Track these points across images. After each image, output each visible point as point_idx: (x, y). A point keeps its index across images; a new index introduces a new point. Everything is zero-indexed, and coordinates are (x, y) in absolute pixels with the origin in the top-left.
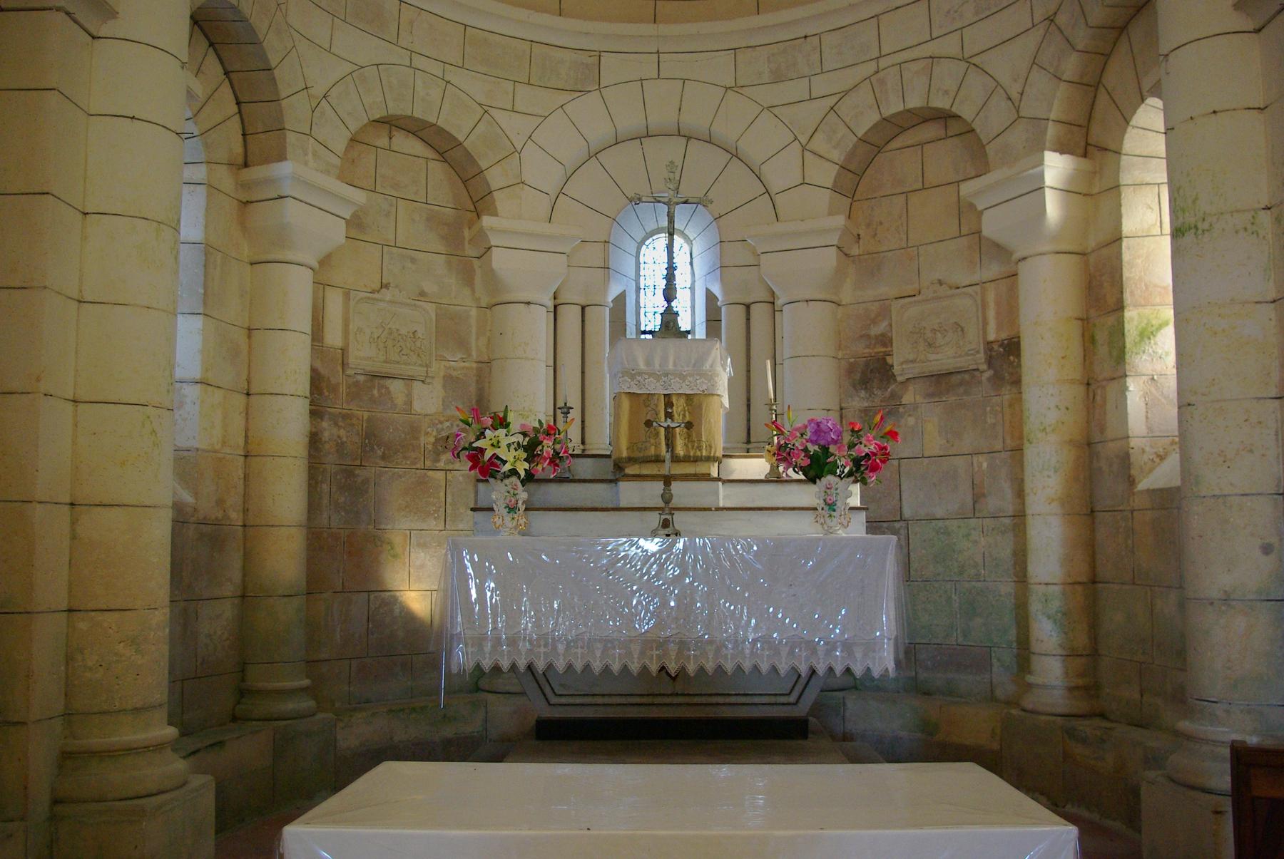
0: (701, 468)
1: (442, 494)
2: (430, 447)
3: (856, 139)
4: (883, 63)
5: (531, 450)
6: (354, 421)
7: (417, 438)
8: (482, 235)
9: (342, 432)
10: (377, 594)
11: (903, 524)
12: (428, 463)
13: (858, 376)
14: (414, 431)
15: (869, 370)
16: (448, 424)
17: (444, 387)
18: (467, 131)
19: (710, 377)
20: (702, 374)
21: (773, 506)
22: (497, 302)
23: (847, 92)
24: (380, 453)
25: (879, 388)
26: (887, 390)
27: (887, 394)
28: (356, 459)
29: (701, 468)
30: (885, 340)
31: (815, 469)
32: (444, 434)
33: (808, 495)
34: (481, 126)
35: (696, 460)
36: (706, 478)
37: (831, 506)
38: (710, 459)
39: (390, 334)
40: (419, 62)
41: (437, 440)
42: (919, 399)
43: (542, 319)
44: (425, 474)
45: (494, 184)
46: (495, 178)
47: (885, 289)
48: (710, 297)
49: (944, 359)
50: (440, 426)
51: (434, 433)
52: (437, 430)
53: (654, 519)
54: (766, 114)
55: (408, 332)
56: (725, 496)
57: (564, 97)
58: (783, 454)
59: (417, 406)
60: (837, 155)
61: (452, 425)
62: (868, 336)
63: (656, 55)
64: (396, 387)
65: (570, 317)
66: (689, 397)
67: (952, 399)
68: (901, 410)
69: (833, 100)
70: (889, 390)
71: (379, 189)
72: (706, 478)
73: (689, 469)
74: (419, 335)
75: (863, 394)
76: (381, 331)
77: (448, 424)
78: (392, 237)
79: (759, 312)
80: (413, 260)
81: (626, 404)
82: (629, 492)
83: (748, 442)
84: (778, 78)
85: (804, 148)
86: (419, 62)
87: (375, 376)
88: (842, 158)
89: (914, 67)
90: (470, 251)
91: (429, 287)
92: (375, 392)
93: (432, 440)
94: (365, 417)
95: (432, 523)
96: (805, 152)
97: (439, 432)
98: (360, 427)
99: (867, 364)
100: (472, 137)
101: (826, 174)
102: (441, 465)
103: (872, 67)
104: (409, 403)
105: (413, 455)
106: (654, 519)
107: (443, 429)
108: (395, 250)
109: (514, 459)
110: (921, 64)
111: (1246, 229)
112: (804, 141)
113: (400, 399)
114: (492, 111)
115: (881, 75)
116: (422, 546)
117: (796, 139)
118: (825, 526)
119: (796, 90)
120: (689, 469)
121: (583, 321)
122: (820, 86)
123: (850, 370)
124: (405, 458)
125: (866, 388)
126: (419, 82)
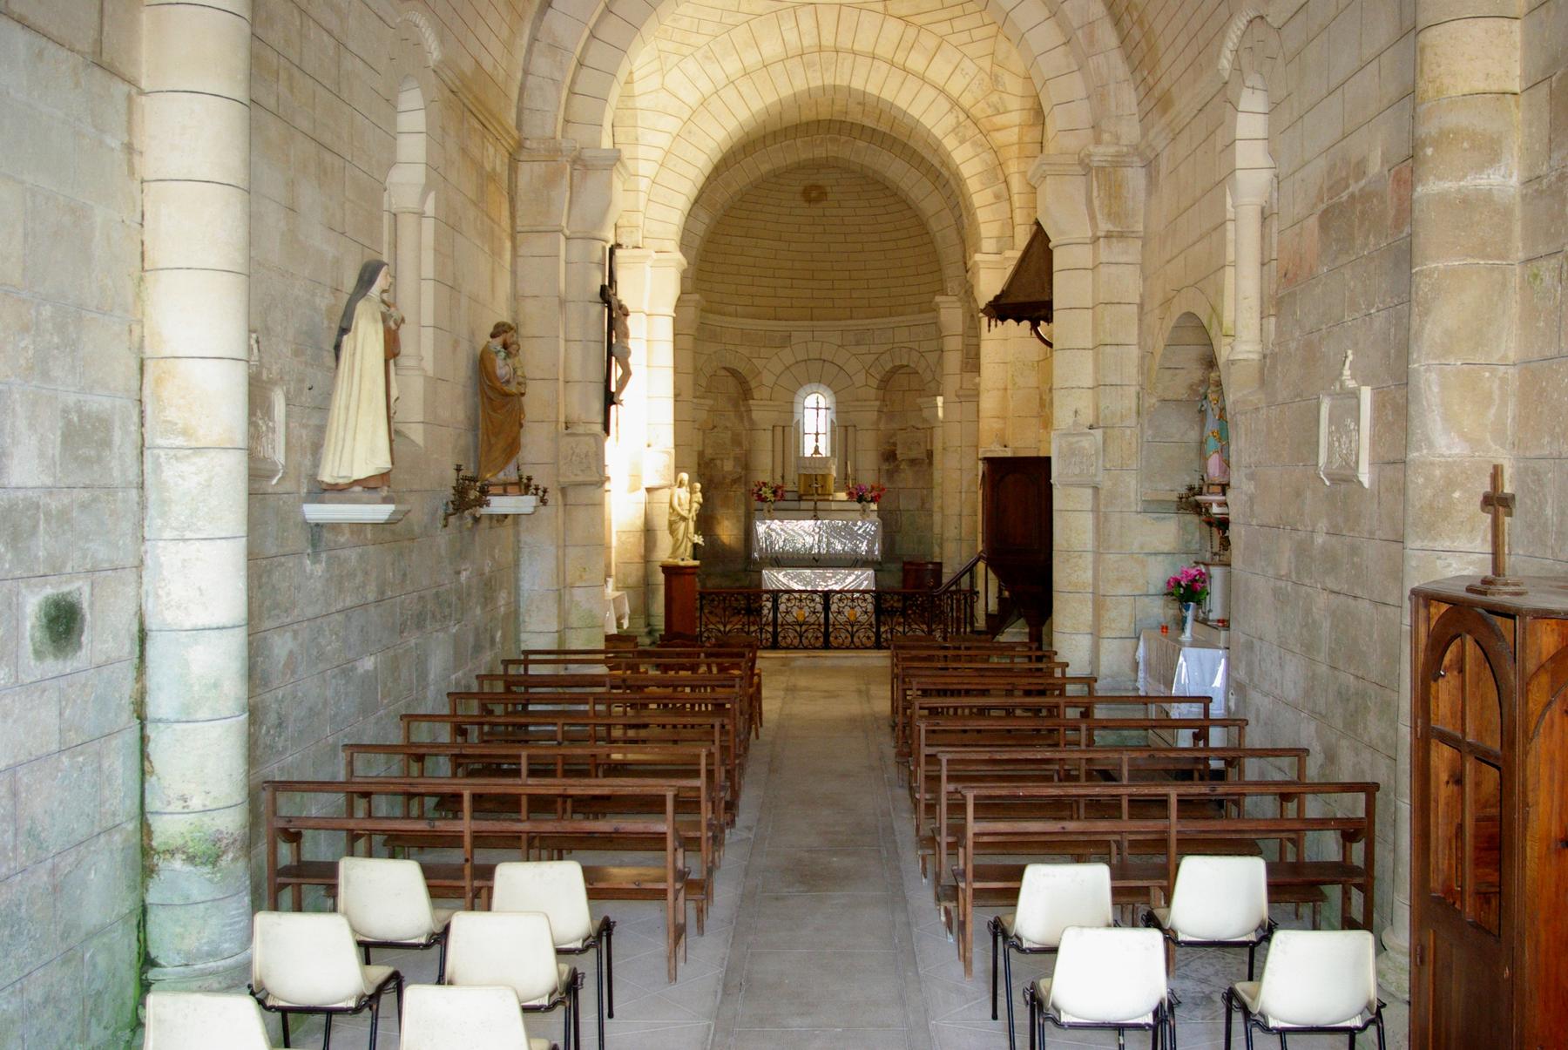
0: (826, 497)
5: (775, 493)
8: (749, 406)
19: (829, 469)
20: (826, 468)
22: (753, 427)
29: (826, 497)
30: (895, 444)
31: (860, 499)
33: (857, 506)
35: (824, 495)
36: (828, 500)
37: (864, 511)
38: (829, 495)
40: (728, 347)
43: (769, 434)
45: (753, 386)
46: (753, 384)
47: (895, 426)
48: (832, 421)
49: (913, 454)
53: (812, 513)
56: (834, 506)
57: (775, 351)
58: (850, 494)
60: (878, 376)
64: (718, 462)
65: (779, 431)
66: (823, 475)
72: (828, 500)
73: (822, 498)
79: (851, 430)
81: (803, 478)
82: (804, 505)
84: (858, 344)
85: (867, 372)
86: (728, 347)
87: (713, 459)
89: (905, 350)
90: (743, 409)
91: (729, 425)
95: (730, 511)
101: (874, 383)
106: (812, 513)
109: (770, 496)
116: (727, 519)
118: (1265, 267)
119: (863, 349)
120: (822, 498)
122: (874, 349)
123: (883, 454)
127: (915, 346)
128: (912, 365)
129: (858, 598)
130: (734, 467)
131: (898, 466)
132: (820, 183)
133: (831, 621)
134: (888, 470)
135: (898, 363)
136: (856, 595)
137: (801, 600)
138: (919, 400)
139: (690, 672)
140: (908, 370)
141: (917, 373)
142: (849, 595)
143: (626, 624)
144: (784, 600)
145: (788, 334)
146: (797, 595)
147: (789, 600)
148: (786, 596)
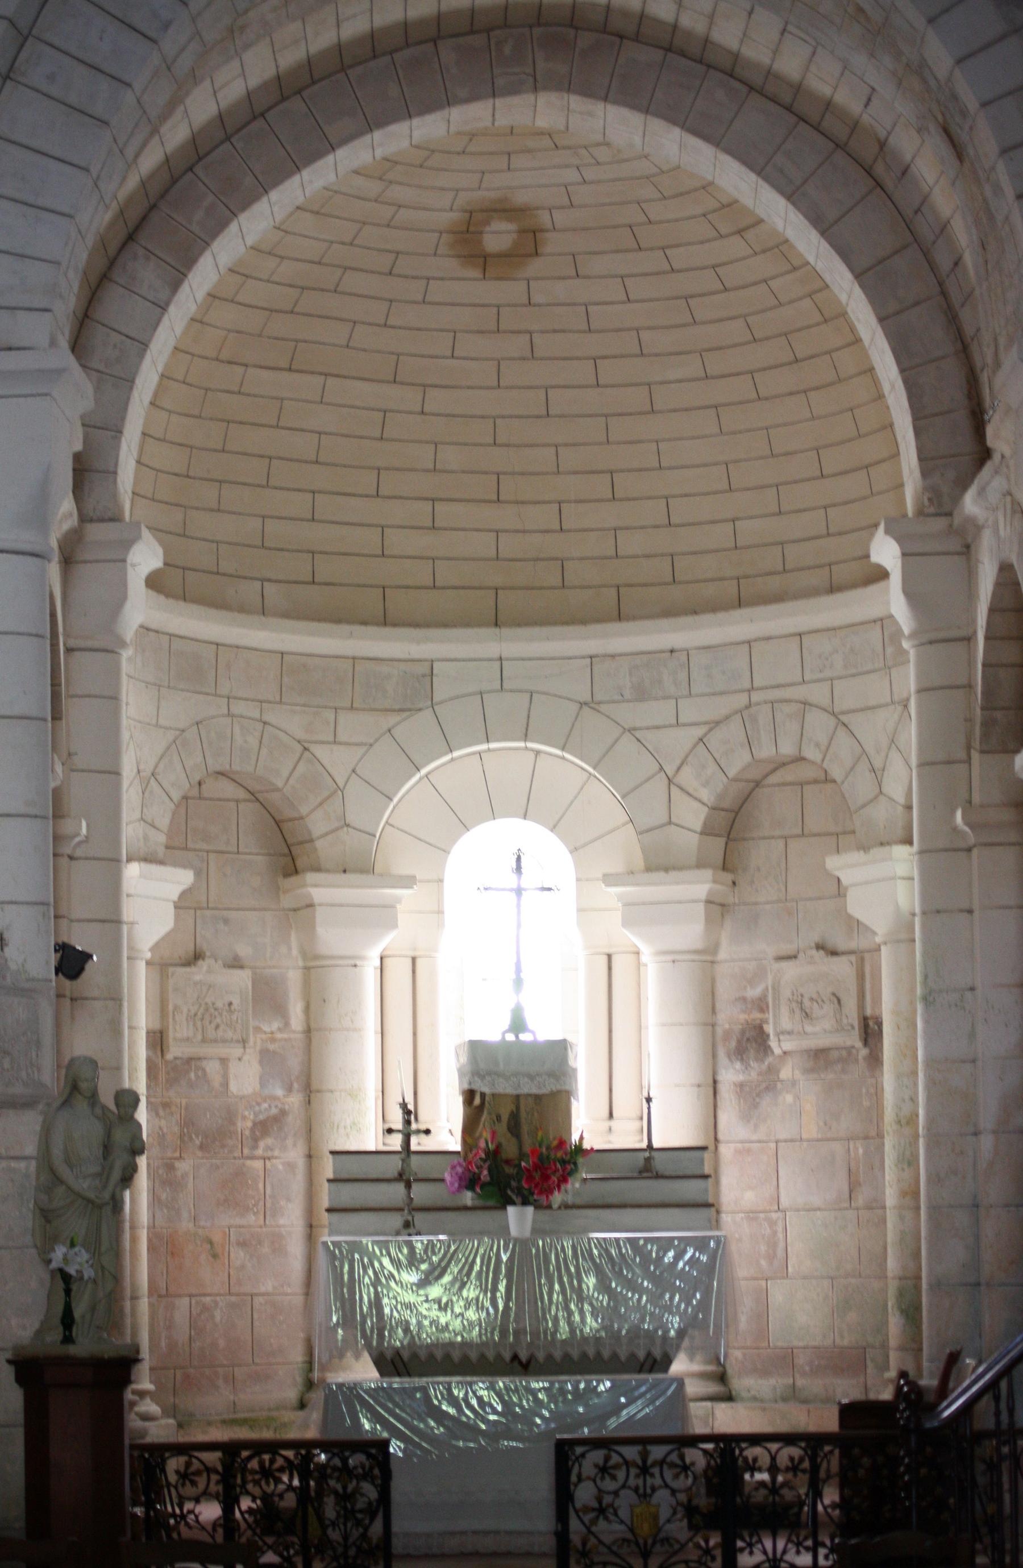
1: (261, 1186)
2: (247, 1133)
3: (725, 780)
4: (756, 697)
6: (174, 1108)
7: (234, 1124)
9: (163, 1123)
10: (198, 1298)
11: (780, 1214)
12: (246, 1151)
13: (733, 1044)
14: (230, 1116)
15: (745, 1039)
16: (265, 1105)
17: (261, 1062)
18: (285, 773)
21: (713, 1126)
23: (717, 723)
24: (198, 1142)
25: (757, 1059)
26: (764, 1063)
27: (764, 1066)
28: (175, 1151)
32: (261, 1117)
34: (301, 768)
39: (207, 1010)
40: (239, 708)
41: (255, 1124)
42: (798, 1074)
44: (244, 1165)
50: (257, 1108)
51: (252, 1117)
52: (254, 1114)
54: (627, 737)
55: (224, 1005)
57: (393, 719)
59: (233, 1087)
60: (705, 795)
61: (270, 1106)
62: (744, 999)
63: (498, 663)
67: (831, 1076)
68: (779, 1085)
69: (700, 731)
70: (766, 1063)
71: (190, 845)
74: (235, 1006)
75: (738, 1065)
76: (196, 1007)
77: (265, 1105)
78: (204, 899)
80: (226, 921)
83: (611, 1115)
84: (641, 695)
86: (239, 708)
88: (712, 799)
92: (192, 1075)
93: (249, 1124)
94: (183, 1104)
96: (672, 786)
97: (256, 1115)
98: (179, 1116)
99: (743, 1032)
100: (291, 782)
102: (260, 1152)
103: (742, 700)
104: (226, 1084)
105: (230, 1142)
107: (260, 1112)
108: (208, 913)
110: (794, 707)
111: (956, 1005)
112: (670, 770)
113: (216, 1081)
114: (313, 748)
115: (753, 710)
117: (662, 768)
119: (659, 711)
121: (414, 972)
124: (223, 1146)
125: (742, 1060)
126: (237, 730)
127: (818, 694)
128: (811, 753)
129: (661, 1463)
130: (263, 1083)
131: (772, 1071)
132: (521, 198)
133: (575, 1539)
134: (741, 1085)
135: (766, 751)
136: (657, 1452)
137: (644, 1470)
138: (833, 863)
139: (142, 1161)
140: (806, 772)
141: (828, 780)
142: (631, 1452)
143: (484, 1338)
144: (173, 1478)
145: (423, 669)
146: (631, 1452)
147: (604, 1470)
148: (597, 1456)
